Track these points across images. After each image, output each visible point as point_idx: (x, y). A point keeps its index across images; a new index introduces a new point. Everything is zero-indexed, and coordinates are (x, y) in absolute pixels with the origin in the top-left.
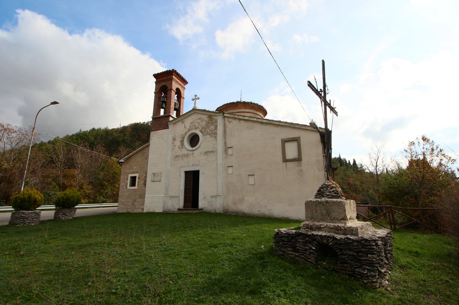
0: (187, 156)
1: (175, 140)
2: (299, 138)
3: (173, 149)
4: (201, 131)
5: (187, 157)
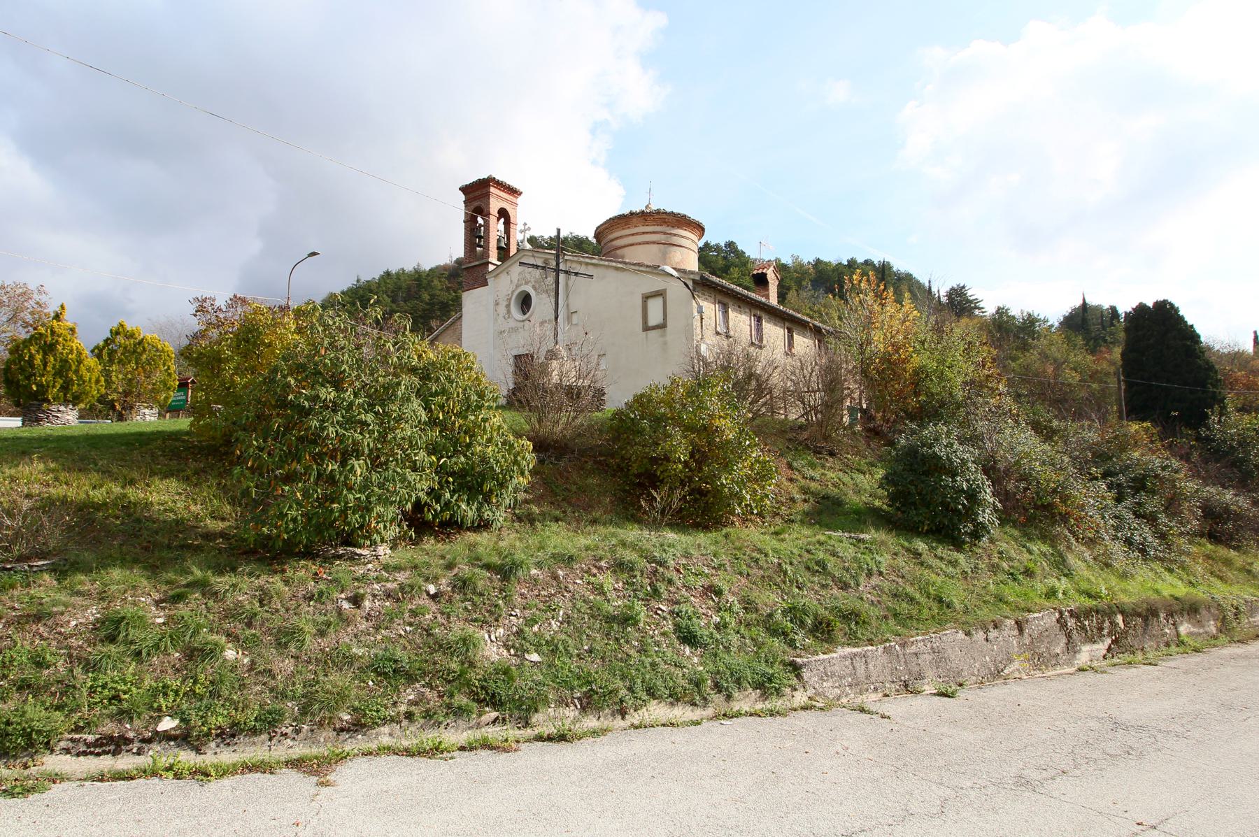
0: (516, 330)
1: (497, 304)
3: (496, 320)
4: (535, 289)
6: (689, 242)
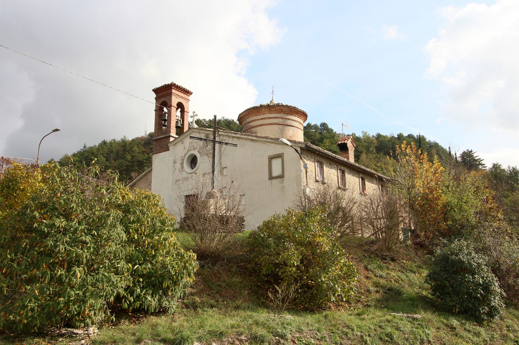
0: (187, 179)
2: (283, 154)
3: (174, 172)
5: (187, 180)
6: (298, 123)
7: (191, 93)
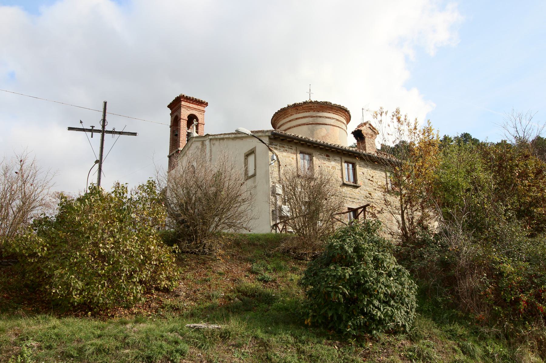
6: (334, 120)
7: (207, 104)
